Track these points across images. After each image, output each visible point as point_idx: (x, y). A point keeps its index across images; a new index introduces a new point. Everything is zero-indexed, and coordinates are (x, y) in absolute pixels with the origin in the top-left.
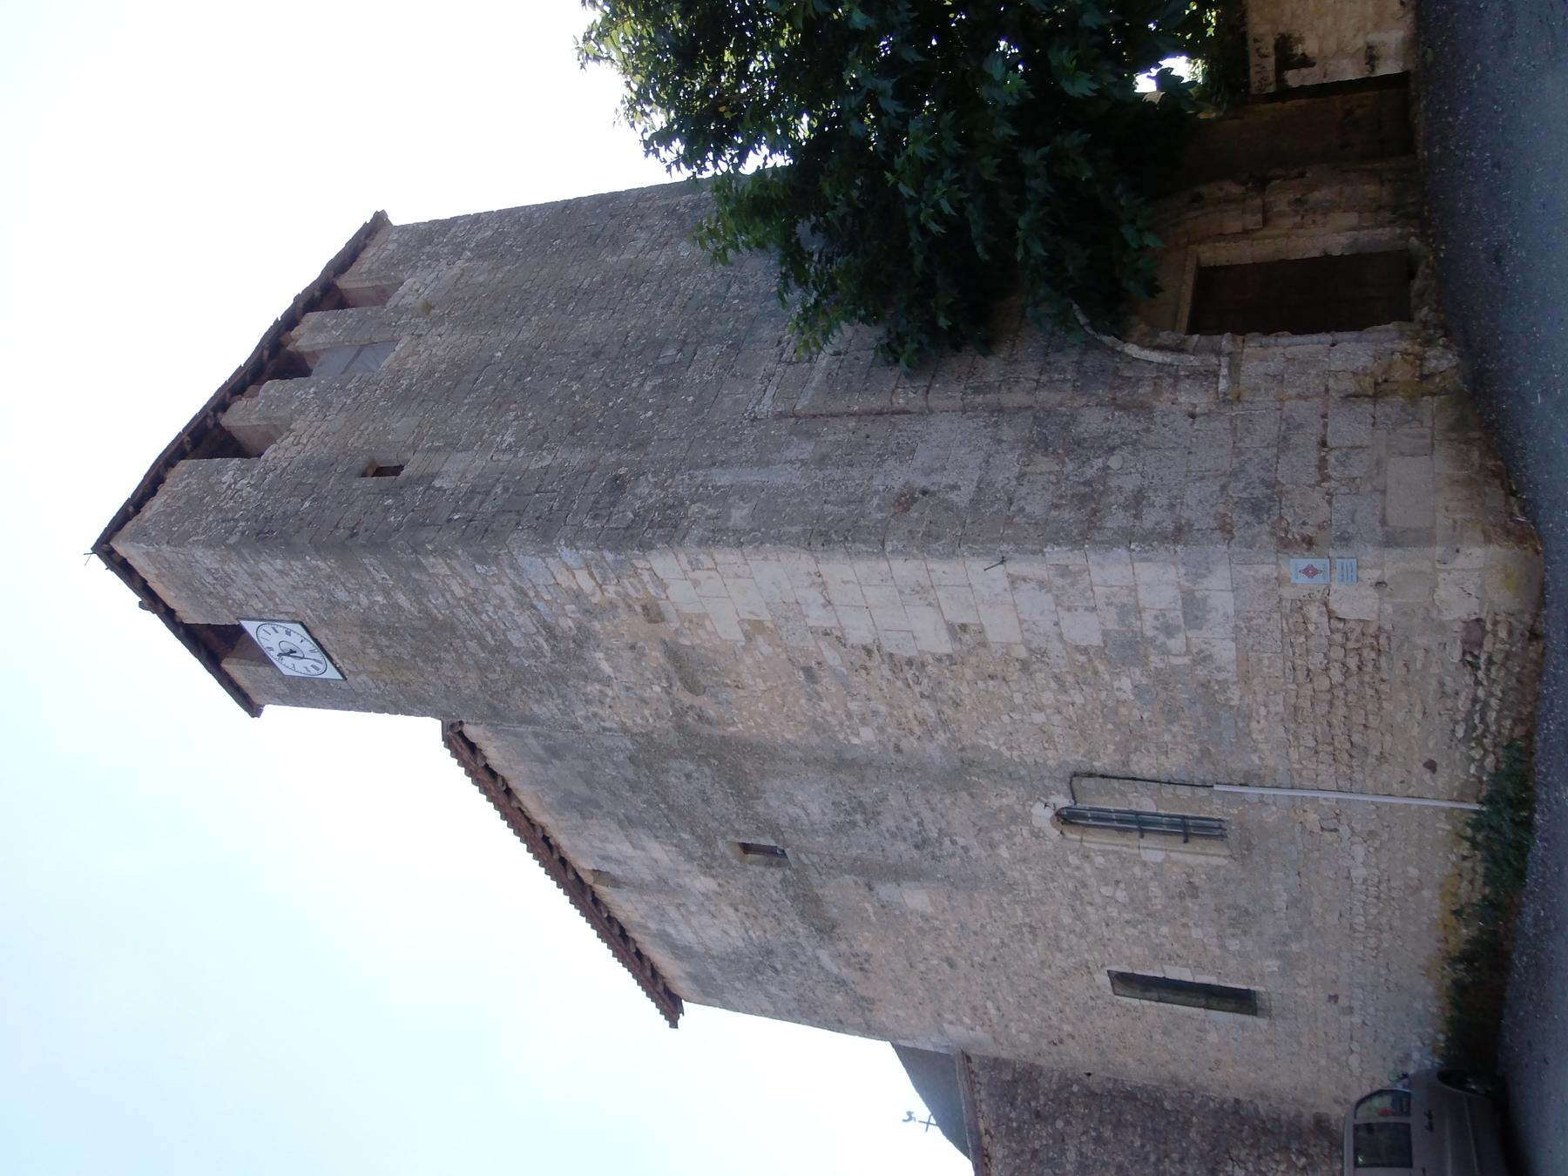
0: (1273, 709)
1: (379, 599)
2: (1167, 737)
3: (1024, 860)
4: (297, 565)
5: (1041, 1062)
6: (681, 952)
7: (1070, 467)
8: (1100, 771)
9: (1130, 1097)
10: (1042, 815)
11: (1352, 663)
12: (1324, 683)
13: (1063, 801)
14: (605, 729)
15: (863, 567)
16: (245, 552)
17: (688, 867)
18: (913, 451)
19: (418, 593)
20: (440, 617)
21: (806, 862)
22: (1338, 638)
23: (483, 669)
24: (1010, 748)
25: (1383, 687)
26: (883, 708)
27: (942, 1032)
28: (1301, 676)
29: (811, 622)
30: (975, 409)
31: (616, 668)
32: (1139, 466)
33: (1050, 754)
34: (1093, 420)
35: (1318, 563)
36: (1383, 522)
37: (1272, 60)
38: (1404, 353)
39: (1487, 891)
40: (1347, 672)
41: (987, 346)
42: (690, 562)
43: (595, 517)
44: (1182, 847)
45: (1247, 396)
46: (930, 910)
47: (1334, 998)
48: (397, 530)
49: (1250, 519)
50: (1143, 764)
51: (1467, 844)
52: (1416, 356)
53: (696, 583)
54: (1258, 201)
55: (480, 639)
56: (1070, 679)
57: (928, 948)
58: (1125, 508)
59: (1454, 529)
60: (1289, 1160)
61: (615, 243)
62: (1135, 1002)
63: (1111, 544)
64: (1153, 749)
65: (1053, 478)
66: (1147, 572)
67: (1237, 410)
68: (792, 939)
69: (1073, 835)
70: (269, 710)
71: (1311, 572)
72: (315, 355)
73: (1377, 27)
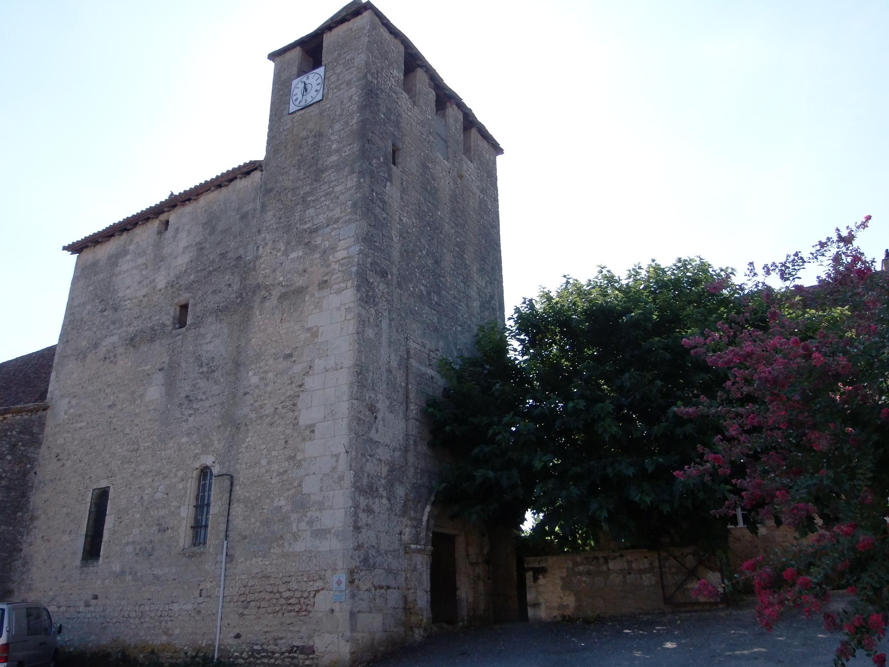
0: (269, 567)
1: (334, 146)
2: (253, 520)
3: (180, 449)
4: (355, 108)
5: (43, 448)
6: (114, 260)
7: (383, 481)
8: (234, 489)
9: (24, 495)
10: (208, 460)
11: (293, 601)
12: (282, 588)
13: (216, 470)
14: (258, 247)
15: (345, 388)
16: (363, 82)
17: (172, 275)
18: (392, 412)
19: (338, 167)
20: (324, 176)
21: (177, 339)
22: (306, 594)
23: (294, 190)
24: (247, 447)
25: (280, 614)
26: (269, 389)
27: (62, 396)
28: (287, 579)
29: (317, 361)
30: (407, 440)
31: (293, 260)
33: (244, 466)
34: (400, 491)
35: (343, 586)
36: (359, 612)
37: (537, 566)
38: (422, 620)
39: (166, 665)
40: (288, 598)
41: (432, 445)
42: (349, 308)
43: (371, 263)
44: (189, 526)
45: (407, 556)
46: (147, 399)
47: (96, 597)
48: (370, 164)
50: (238, 509)
51: (194, 654)
52: (420, 625)
53: (338, 309)
55: (310, 193)
56: (285, 478)
57: (121, 396)
58: (367, 506)
61: (481, 270)
62: (89, 499)
63: (353, 499)
64: (246, 514)
66: (340, 514)
67: (402, 552)
68: (125, 324)
69: (195, 474)
70: (271, 65)
71: (339, 583)
72: (444, 116)
73: (547, 607)
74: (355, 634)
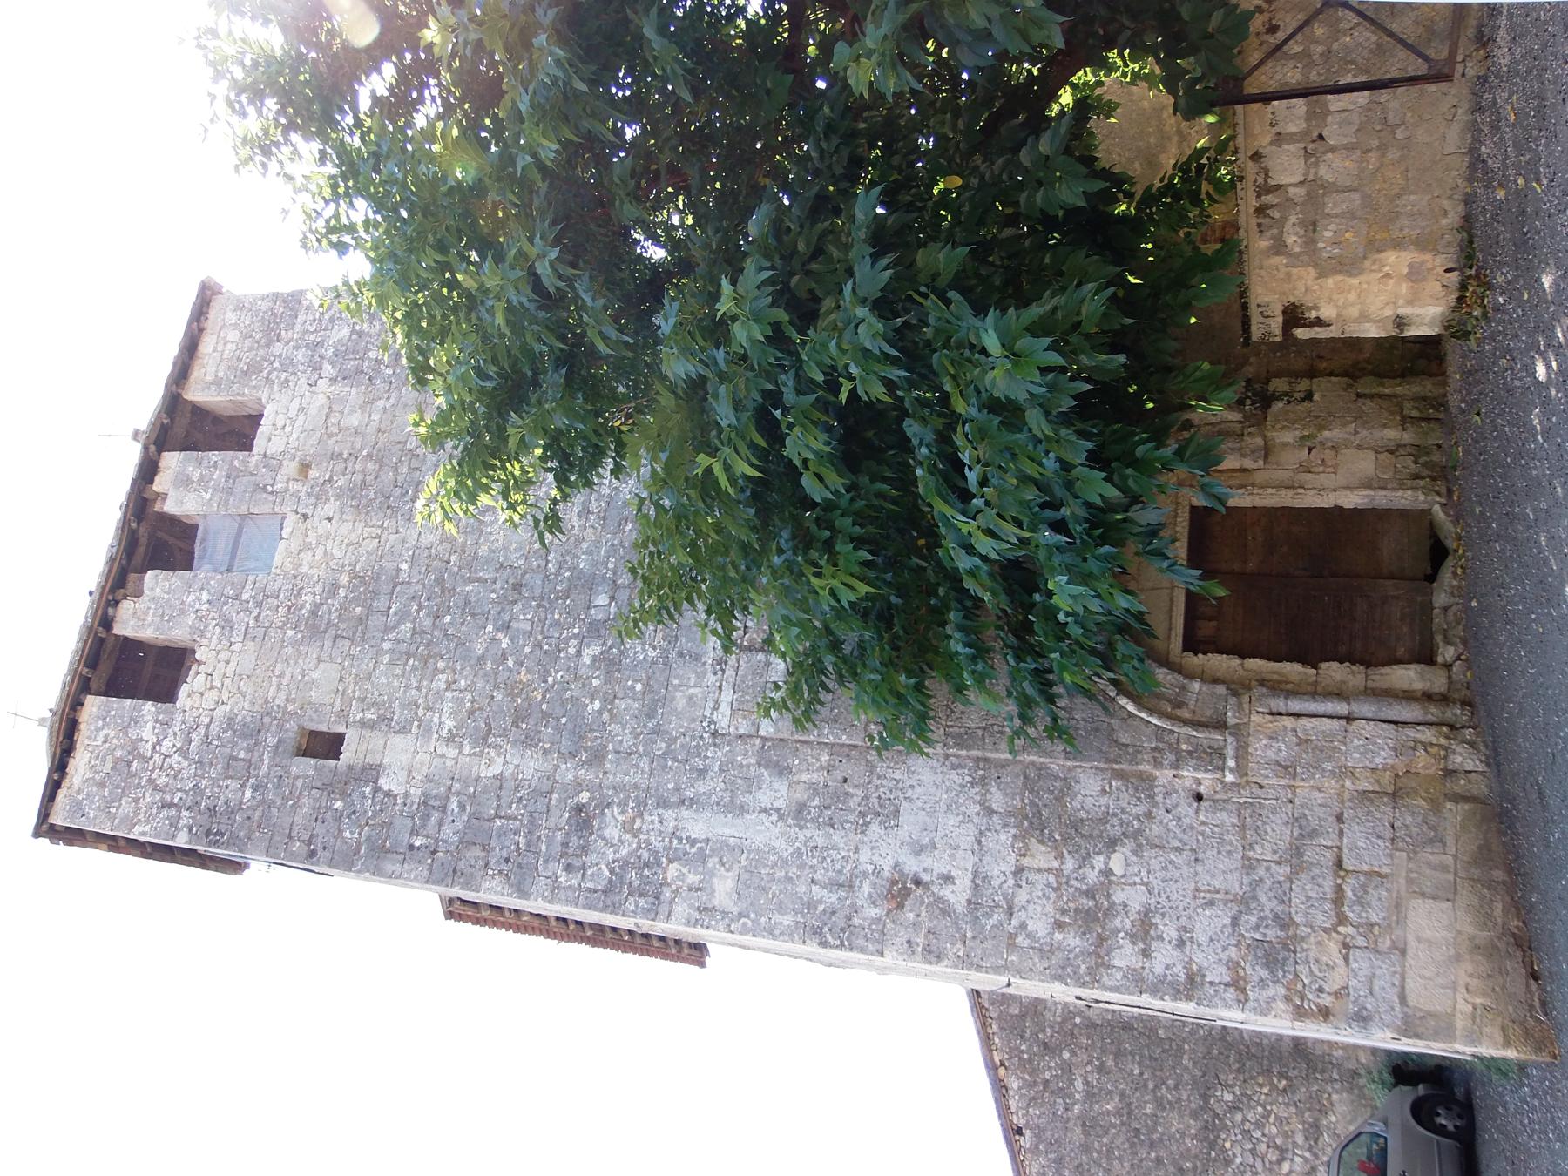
18: (897, 813)
32: (1144, 873)
36: (1403, 999)
37: (1280, 319)
49: (1265, 974)
54: (1259, 441)
59: (1474, 1018)
60: (1271, 1083)
65: (1052, 879)
74: (1460, 1023)
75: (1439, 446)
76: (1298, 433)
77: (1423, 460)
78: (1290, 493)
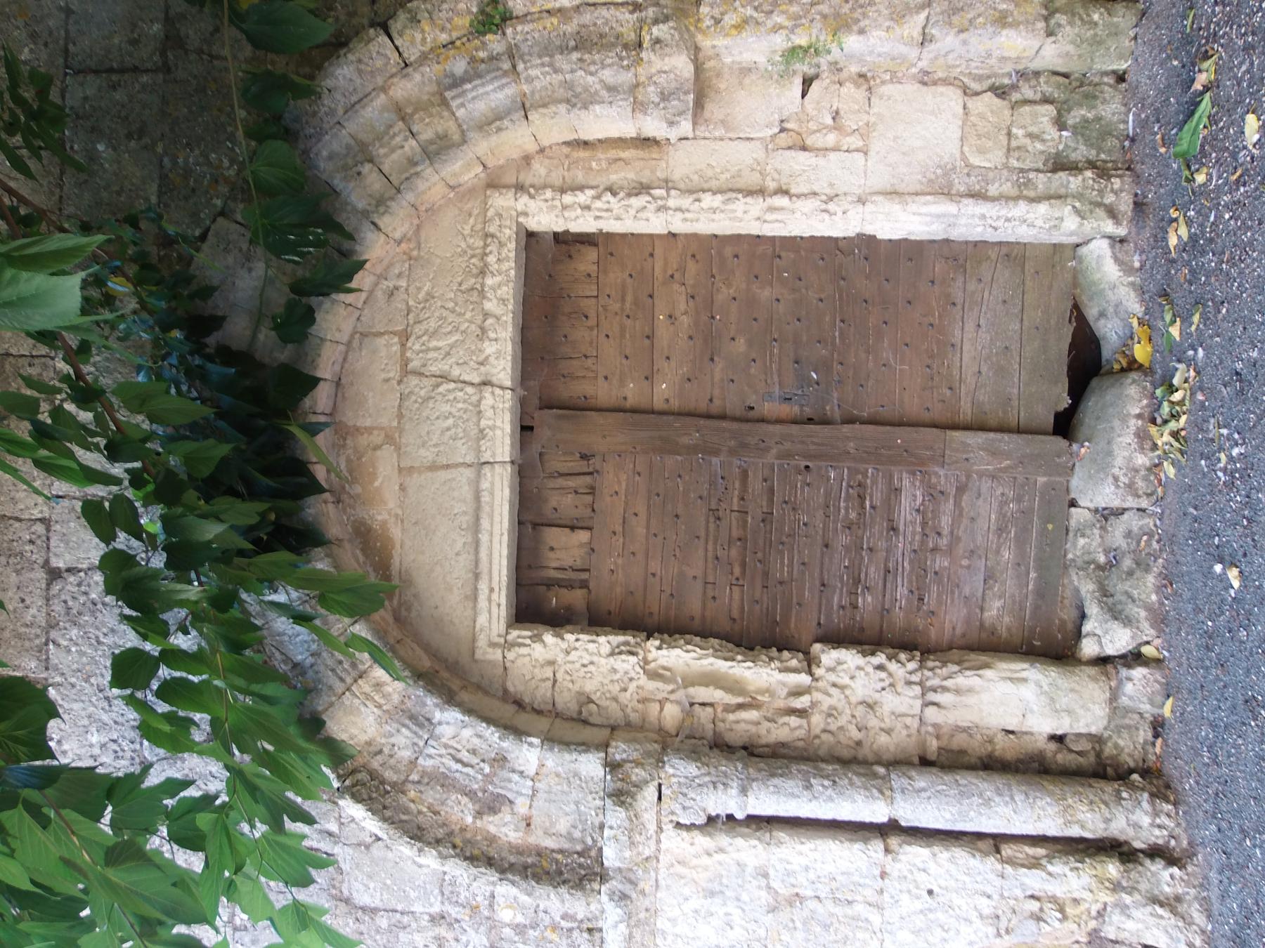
54: (681, 64)
75: (1121, 78)
76: (780, 42)
77: (1076, 115)
78: (756, 206)
